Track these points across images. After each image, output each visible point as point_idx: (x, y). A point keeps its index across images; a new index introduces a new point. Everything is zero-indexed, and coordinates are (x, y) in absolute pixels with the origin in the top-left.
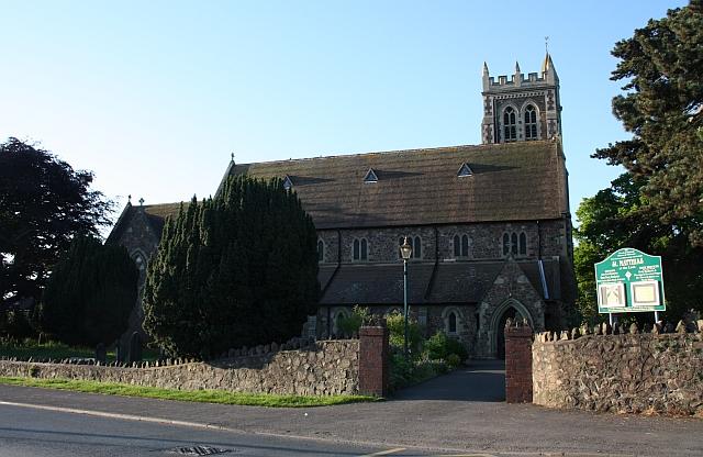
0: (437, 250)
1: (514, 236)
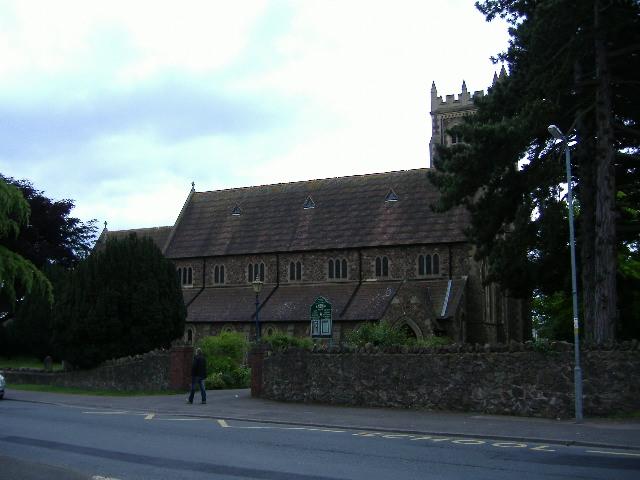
0: (361, 271)
1: (428, 257)
